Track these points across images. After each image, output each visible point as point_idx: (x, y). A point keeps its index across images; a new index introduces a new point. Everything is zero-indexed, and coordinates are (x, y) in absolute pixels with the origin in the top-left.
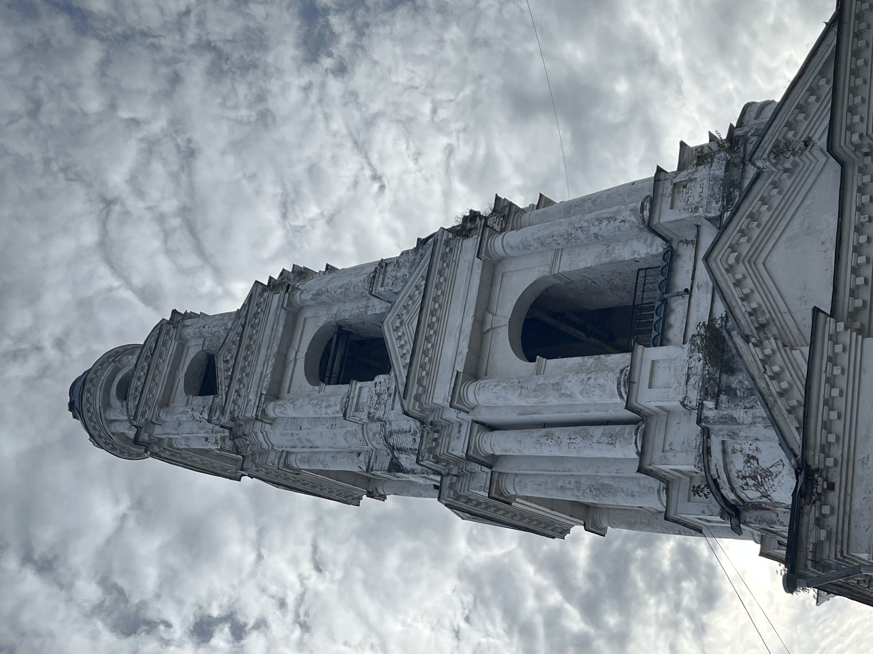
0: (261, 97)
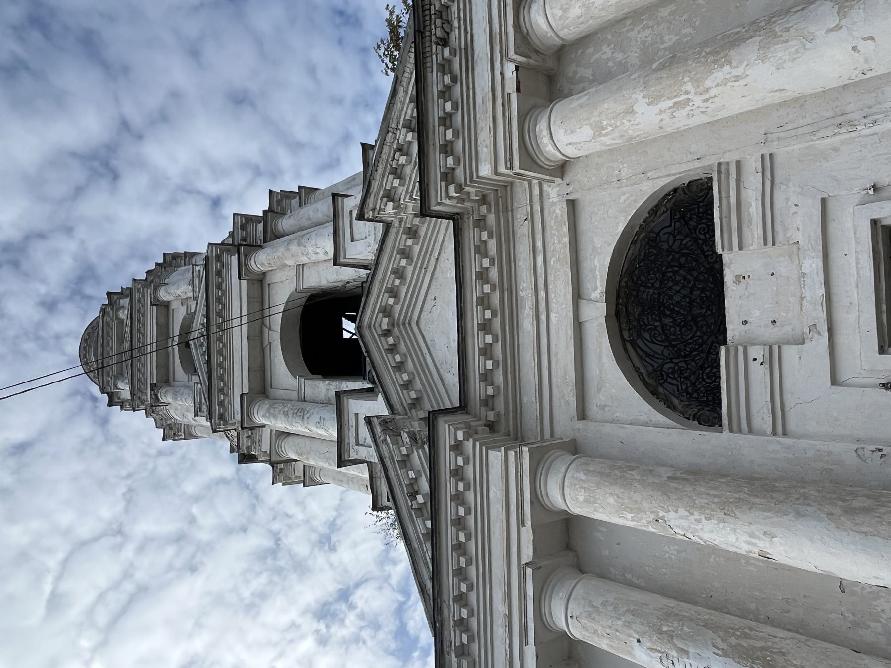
0: (263, 596)
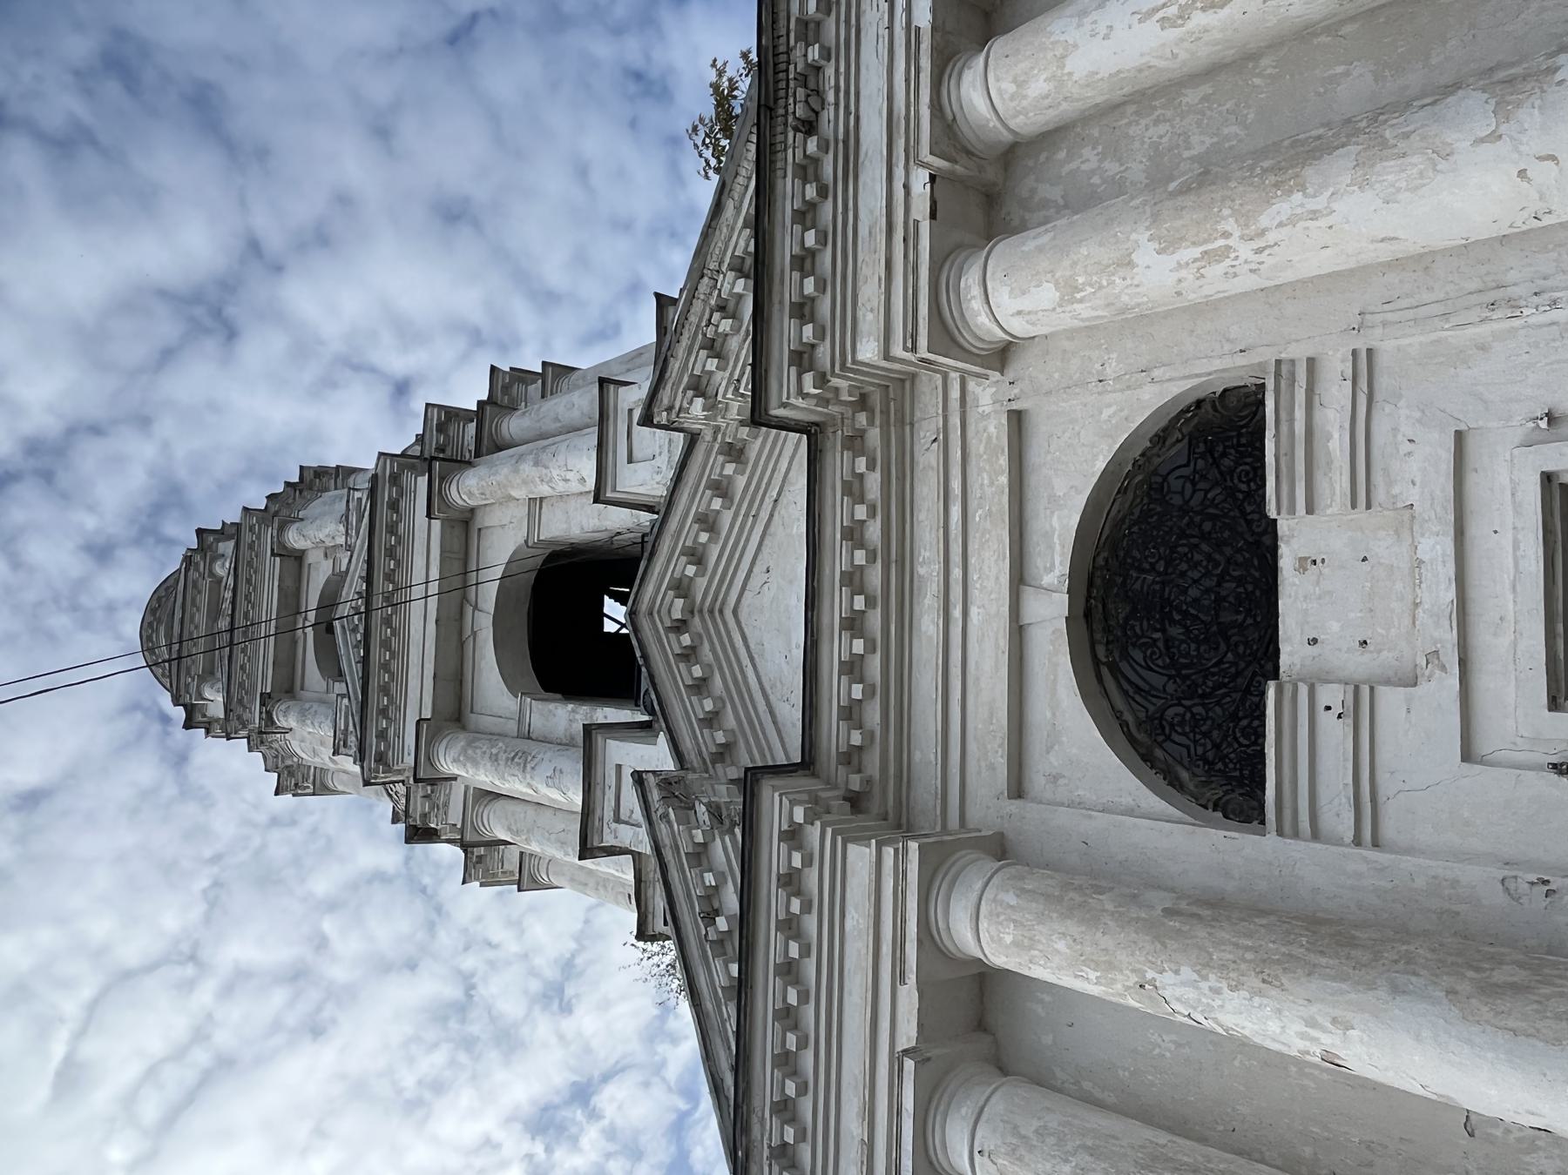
0: (438, 1087)
